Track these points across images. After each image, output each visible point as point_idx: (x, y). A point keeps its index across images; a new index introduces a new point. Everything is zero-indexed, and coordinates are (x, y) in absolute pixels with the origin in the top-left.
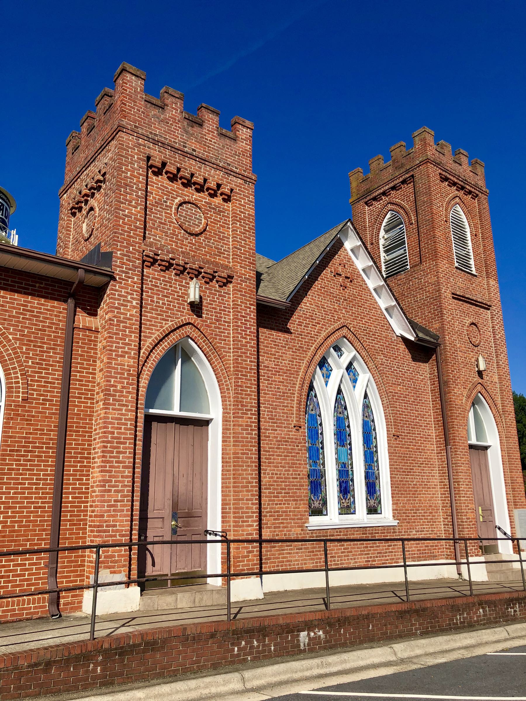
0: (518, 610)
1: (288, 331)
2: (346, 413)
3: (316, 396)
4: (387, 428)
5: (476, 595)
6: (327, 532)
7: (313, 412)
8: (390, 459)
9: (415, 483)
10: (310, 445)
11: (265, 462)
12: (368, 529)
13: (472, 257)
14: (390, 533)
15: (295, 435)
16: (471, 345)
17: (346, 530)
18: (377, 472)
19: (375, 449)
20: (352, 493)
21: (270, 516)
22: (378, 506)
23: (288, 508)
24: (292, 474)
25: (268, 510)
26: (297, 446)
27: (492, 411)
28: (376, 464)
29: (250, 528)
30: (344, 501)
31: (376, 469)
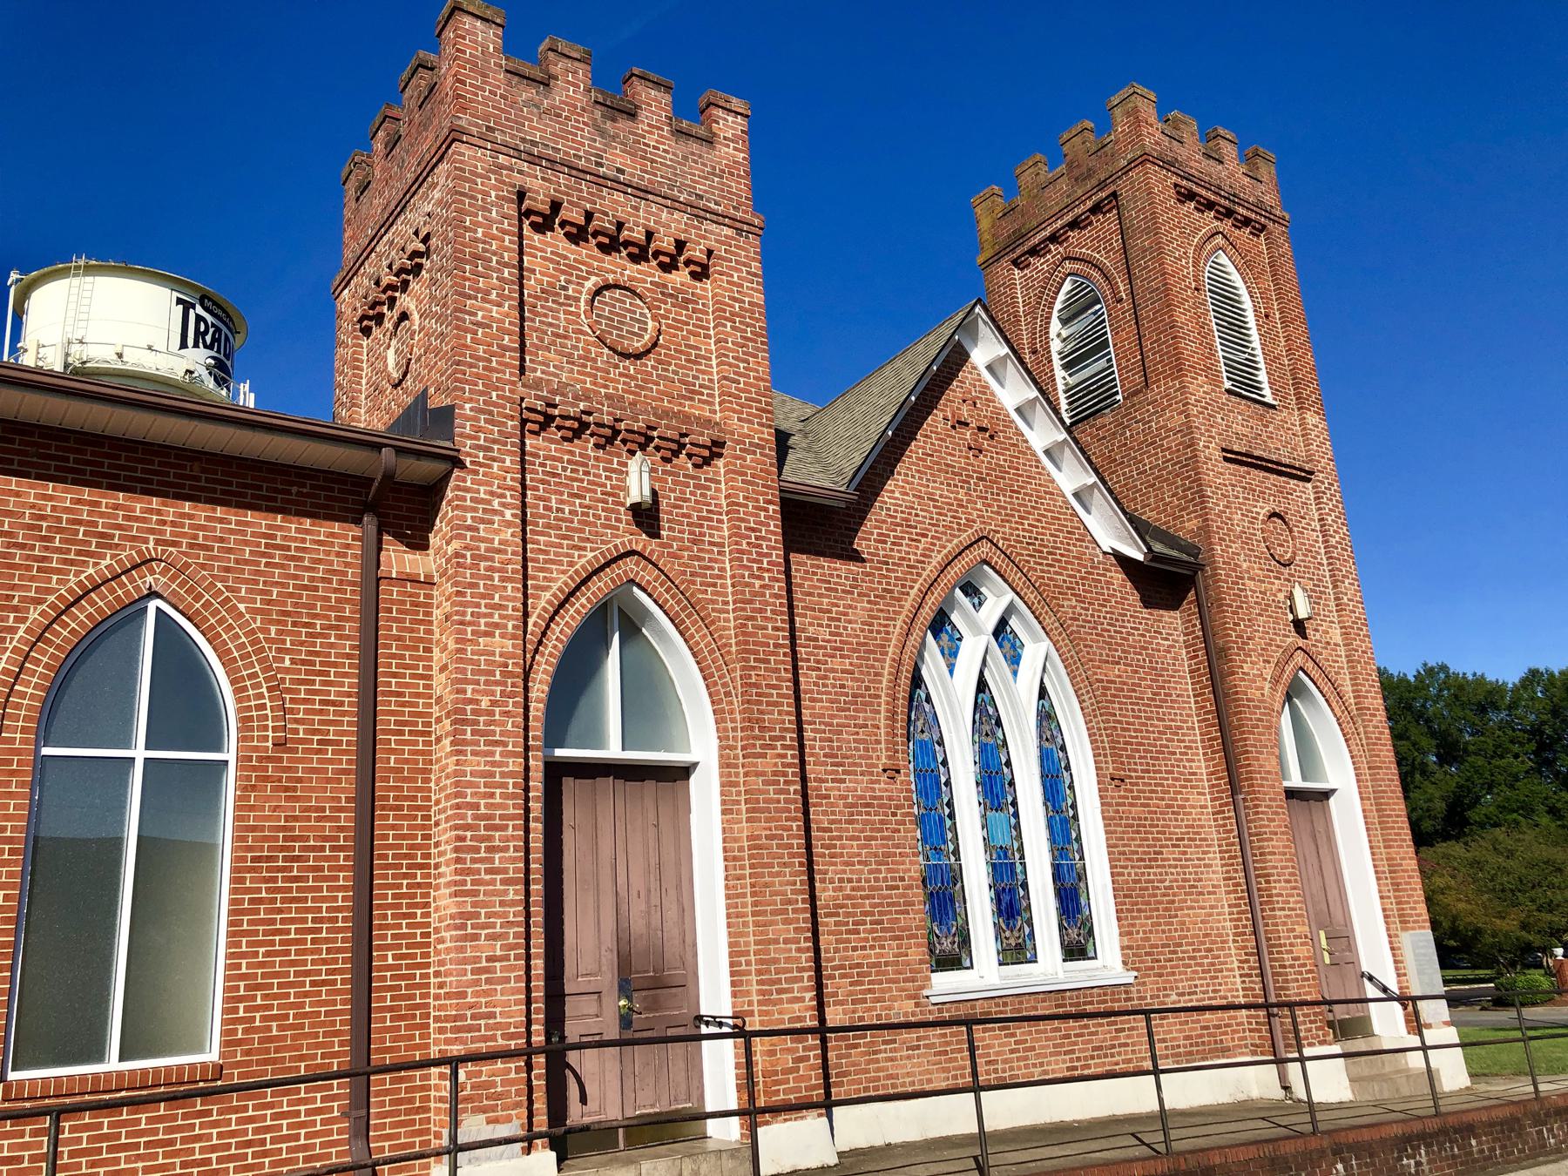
0: (1424, 1160)
1: (856, 557)
2: (1000, 734)
3: (928, 699)
4: (1096, 762)
5: (1324, 1133)
7: (926, 736)
8: (1107, 832)
9: (1167, 884)
11: (823, 855)
12: (1068, 994)
13: (1262, 365)
16: (1273, 563)
17: (1017, 1000)
19: (1071, 813)
20: (1026, 915)
21: (843, 976)
24: (885, 879)
25: (837, 963)
27: (1332, 710)
28: (1076, 846)
29: (796, 1006)
30: (1008, 933)
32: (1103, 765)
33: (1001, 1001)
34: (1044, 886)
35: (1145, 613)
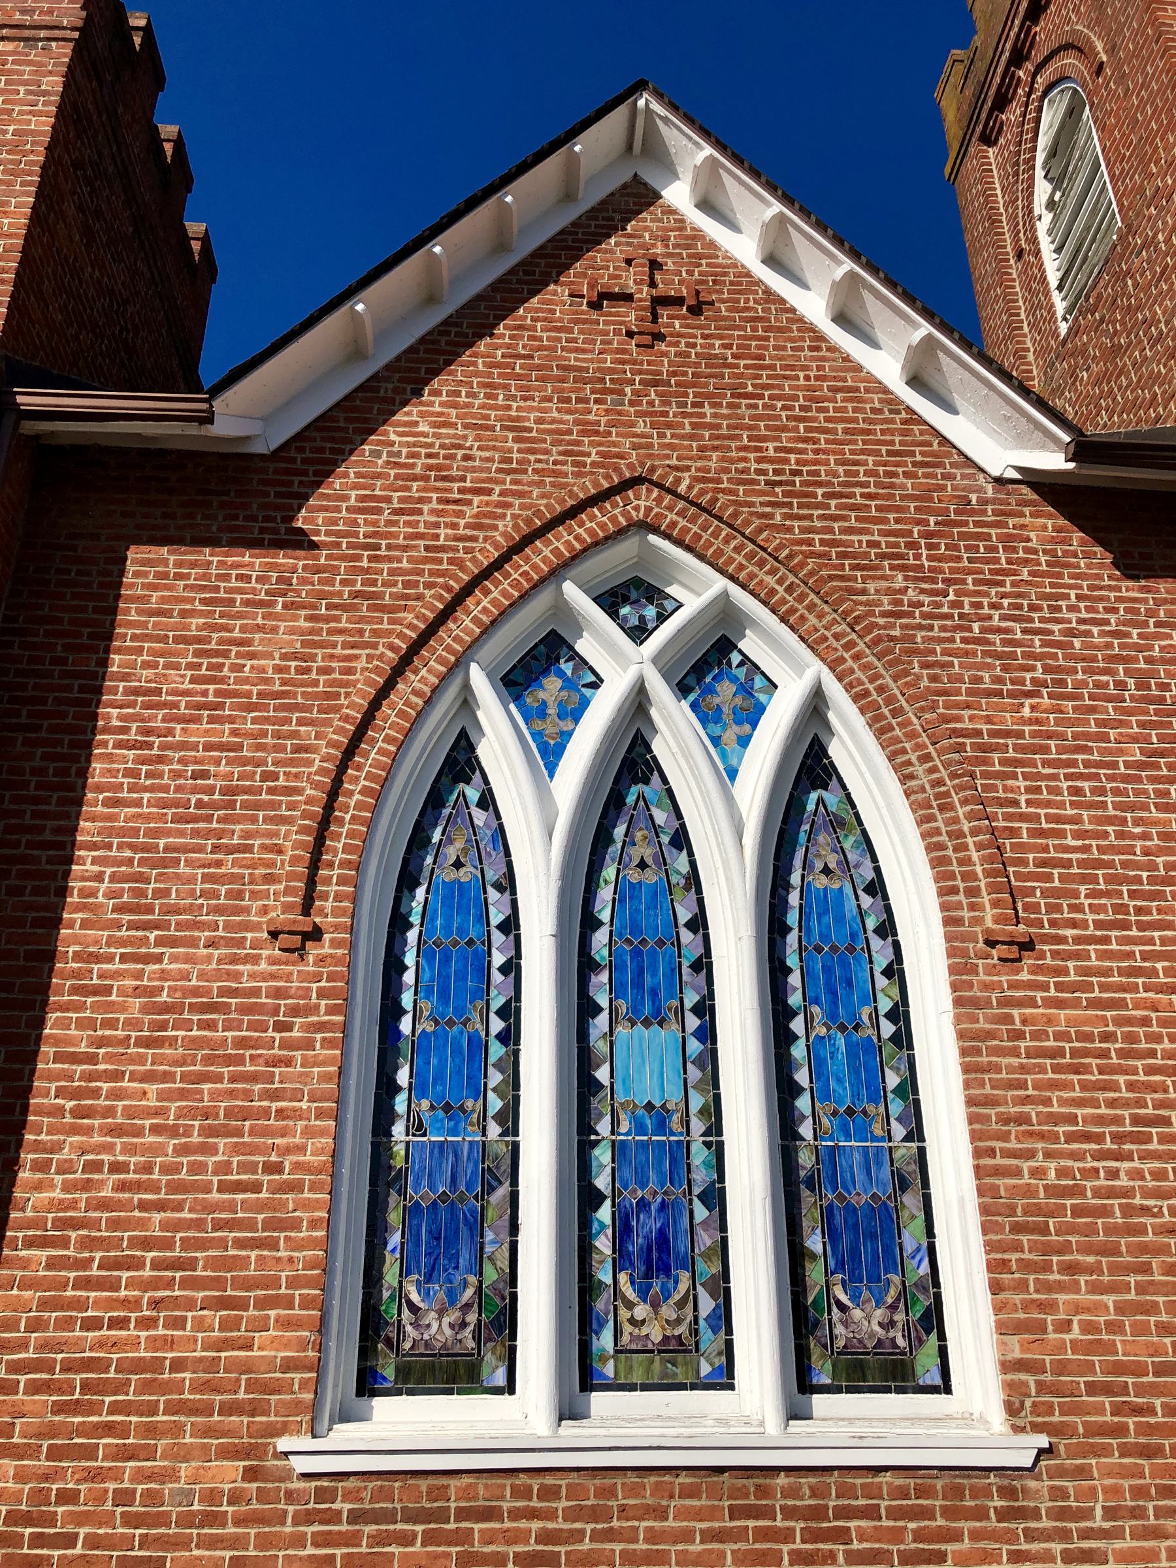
1: (301, 541)
2: (681, 863)
3: (487, 801)
4: (944, 907)
6: (440, 1493)
7: (464, 875)
8: (966, 1069)
10: (427, 1026)
12: (782, 1480)
14: (980, 1514)
15: (273, 977)
17: (592, 1484)
18: (905, 1151)
20: (707, 1269)
21: (35, 1388)
22: (916, 1343)
23: (170, 1343)
26: (281, 1027)
28: (896, 1107)
31: (898, 1131)
32: (966, 914)
33: (535, 1483)
34: (961, 1201)
35: (1129, 588)
